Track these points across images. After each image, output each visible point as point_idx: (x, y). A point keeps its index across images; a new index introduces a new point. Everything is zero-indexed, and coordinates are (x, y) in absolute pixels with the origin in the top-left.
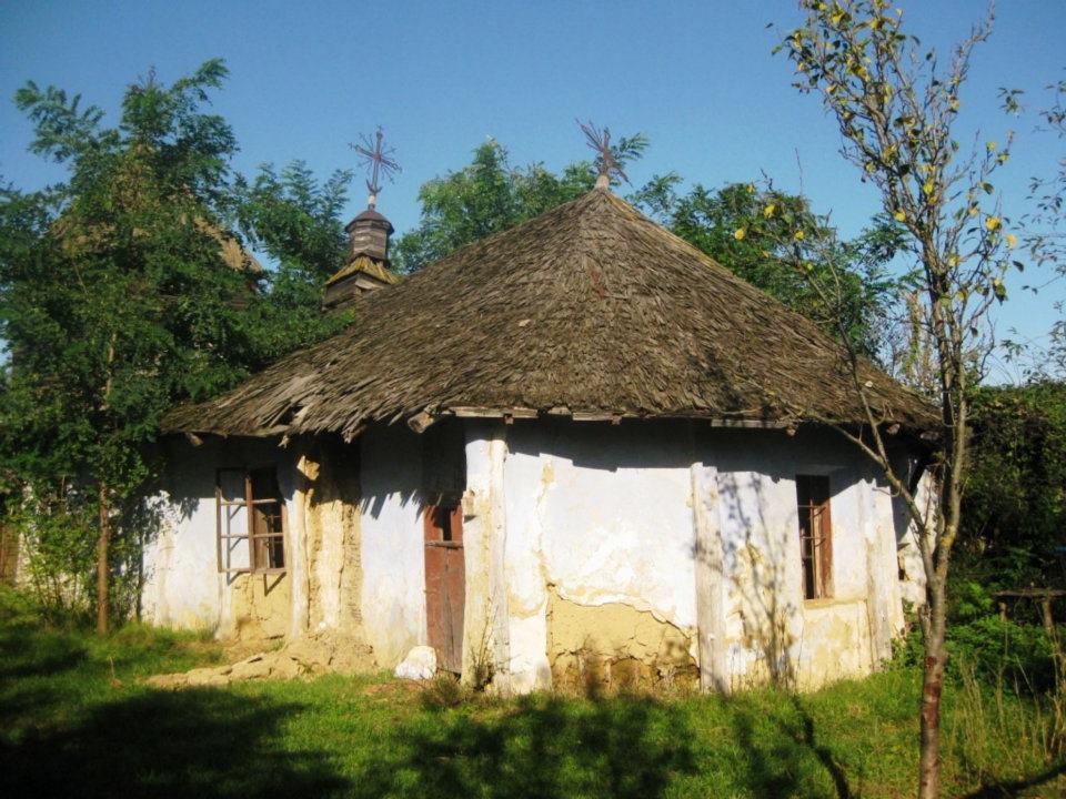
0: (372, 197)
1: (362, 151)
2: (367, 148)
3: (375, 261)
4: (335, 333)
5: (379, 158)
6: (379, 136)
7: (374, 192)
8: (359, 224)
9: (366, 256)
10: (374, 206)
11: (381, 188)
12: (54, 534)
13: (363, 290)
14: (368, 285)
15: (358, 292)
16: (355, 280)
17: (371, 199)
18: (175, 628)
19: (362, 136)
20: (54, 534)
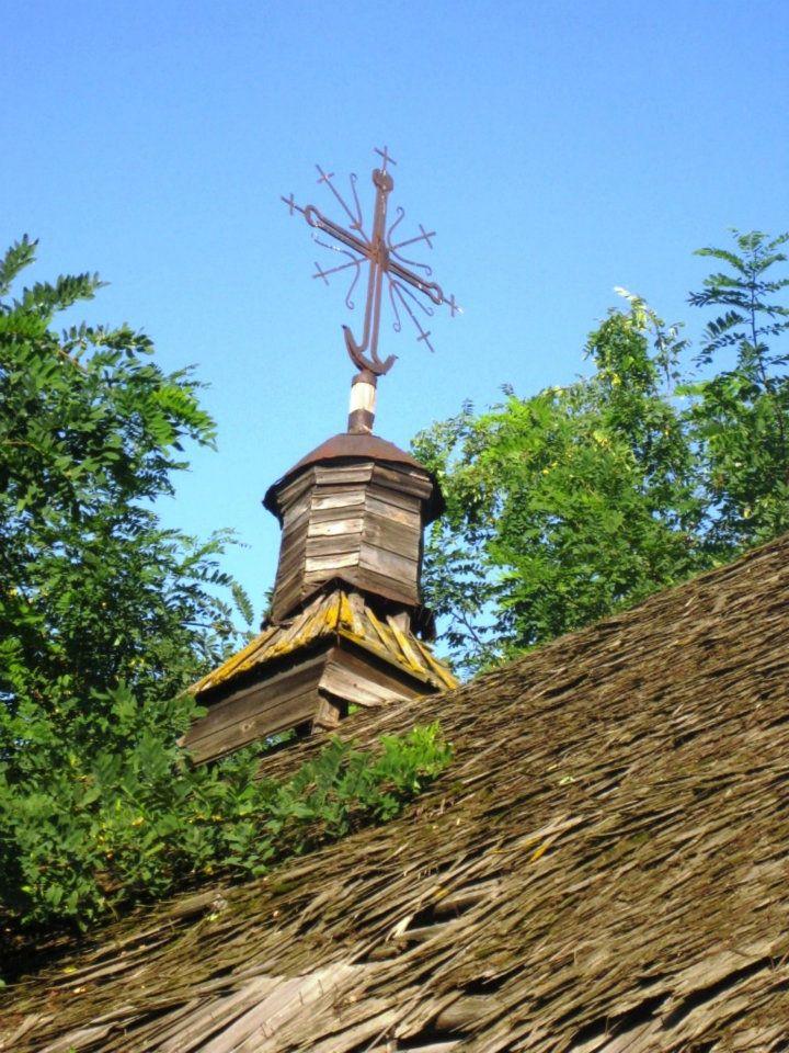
0: (363, 389)
1: (329, 227)
2: (344, 222)
3: (382, 607)
4: (365, 819)
5: (380, 255)
6: (382, 183)
7: (371, 370)
8: (323, 476)
9: (347, 588)
10: (369, 418)
11: (391, 361)
12: (220, 788)
13: (341, 705)
14: (367, 692)
15: (328, 715)
16: (318, 672)
17: (361, 396)
18: (53, 318)
19: (325, 178)
20: (220, 788)
